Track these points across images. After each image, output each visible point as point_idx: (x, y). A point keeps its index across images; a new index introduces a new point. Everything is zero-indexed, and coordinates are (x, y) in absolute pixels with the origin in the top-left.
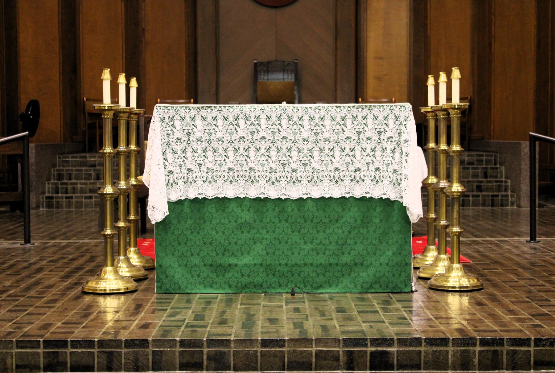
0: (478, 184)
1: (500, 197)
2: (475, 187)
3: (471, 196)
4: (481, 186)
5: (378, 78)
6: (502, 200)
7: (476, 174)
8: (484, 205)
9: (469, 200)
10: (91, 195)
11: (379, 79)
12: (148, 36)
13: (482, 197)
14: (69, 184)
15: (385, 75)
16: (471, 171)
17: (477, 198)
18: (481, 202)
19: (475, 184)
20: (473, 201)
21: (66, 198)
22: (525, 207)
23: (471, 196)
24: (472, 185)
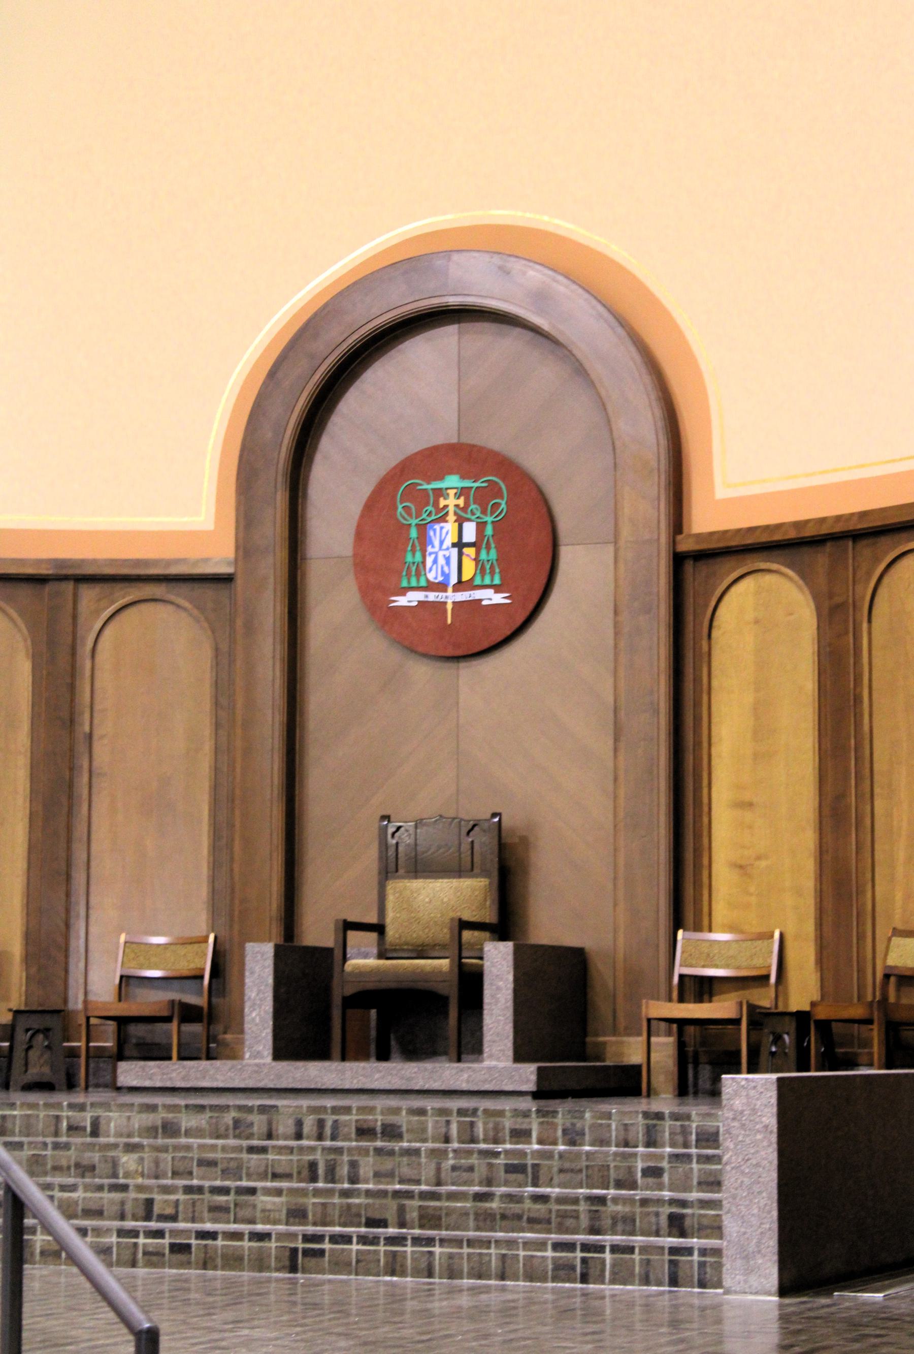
0: (674, 1210)
1: (696, 1257)
2: (664, 1221)
3: (608, 1249)
4: (682, 1217)
5: (741, 867)
6: (702, 1265)
7: (712, 1179)
8: (646, 1281)
9: (603, 1261)
10: (319, 1229)
11: (742, 868)
12: (102, 753)
13: (640, 1254)
14: (206, 1190)
15: (759, 858)
16: (695, 1166)
17: (627, 1256)
18: (637, 1270)
19: (666, 1210)
20: (613, 1265)
21: (121, 1233)
22: (736, 1292)
23: (608, 1249)
24: (657, 1214)
